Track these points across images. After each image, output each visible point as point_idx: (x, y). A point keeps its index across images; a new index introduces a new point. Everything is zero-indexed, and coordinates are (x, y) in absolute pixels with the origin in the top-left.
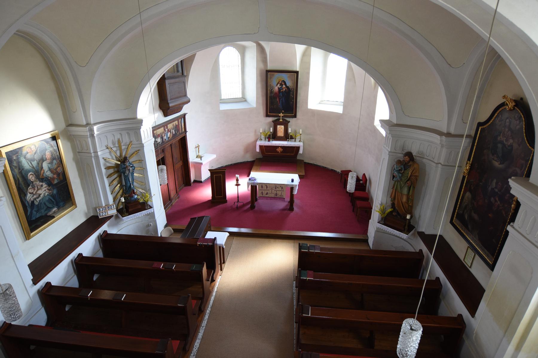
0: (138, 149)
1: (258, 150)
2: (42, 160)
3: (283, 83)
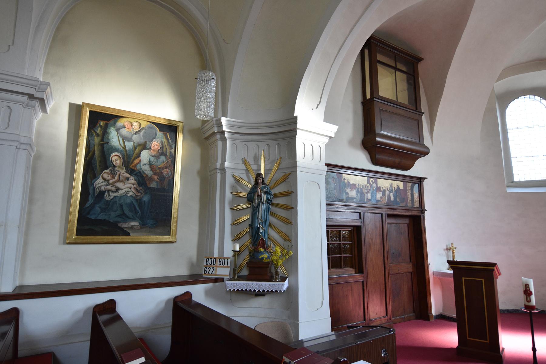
0: (289, 171)
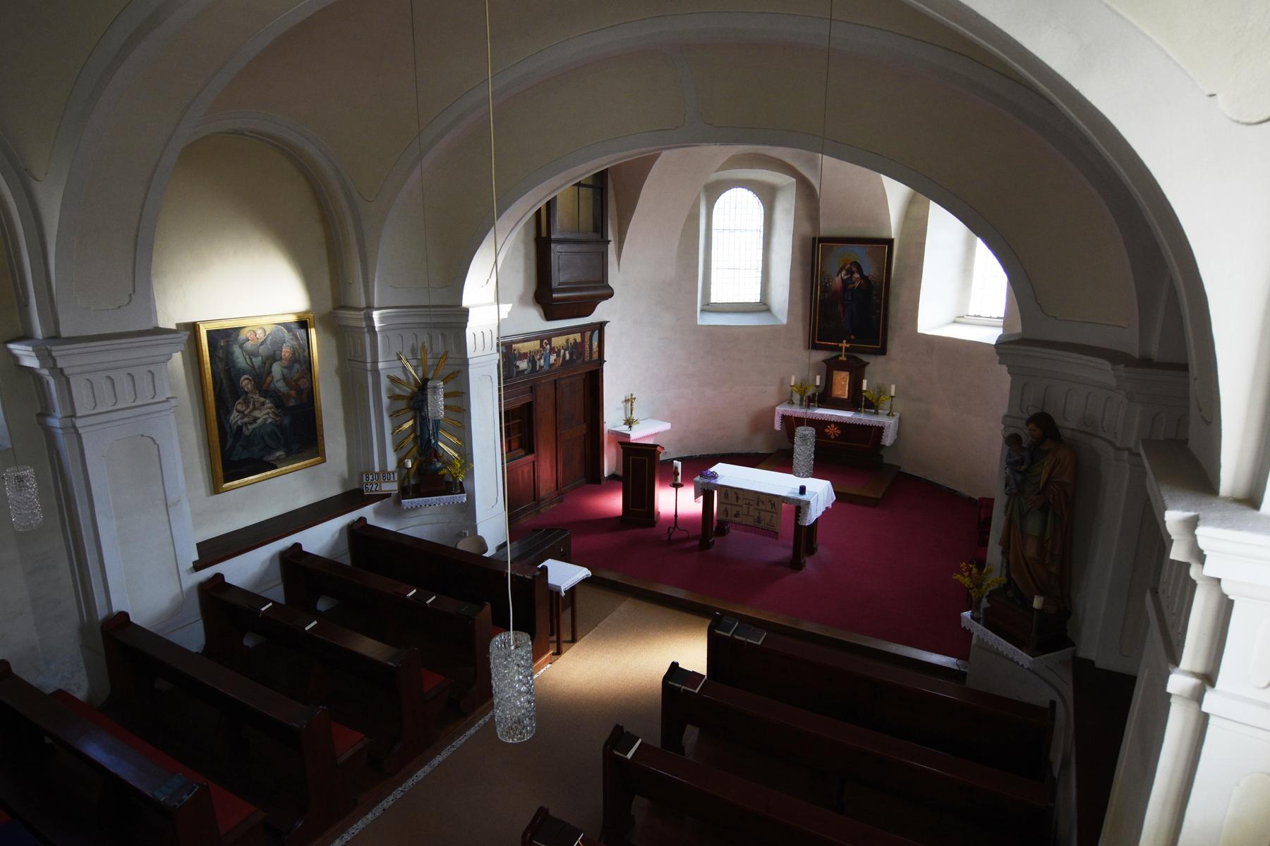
0: (457, 368)
1: (777, 426)
2: (273, 358)
3: (854, 269)
